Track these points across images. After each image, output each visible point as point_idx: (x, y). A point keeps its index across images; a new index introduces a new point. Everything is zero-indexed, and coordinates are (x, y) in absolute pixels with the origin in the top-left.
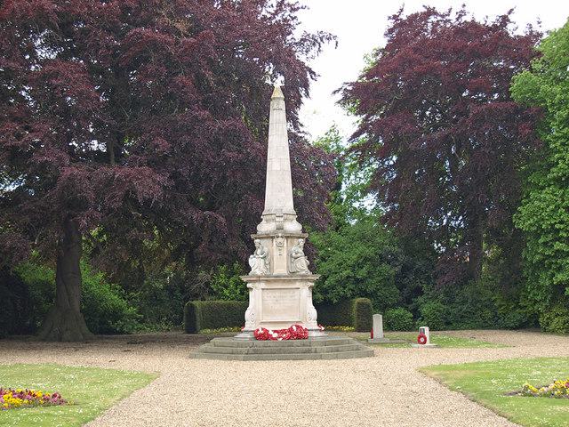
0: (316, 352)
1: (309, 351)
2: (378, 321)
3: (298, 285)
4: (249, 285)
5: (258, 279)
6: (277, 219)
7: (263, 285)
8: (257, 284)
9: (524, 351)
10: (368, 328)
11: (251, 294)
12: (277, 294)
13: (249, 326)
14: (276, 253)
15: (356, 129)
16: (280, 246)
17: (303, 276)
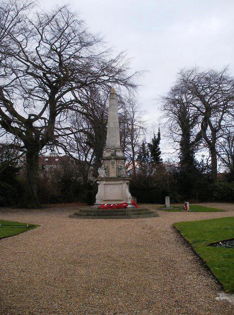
0: (128, 215)
1: (125, 215)
2: (167, 200)
3: (121, 182)
4: (98, 182)
5: (102, 179)
6: (112, 151)
7: (104, 182)
8: (101, 182)
9: (211, 215)
10: (163, 202)
11: (99, 186)
12: (113, 186)
13: (98, 202)
14: (111, 166)
15: (39, 126)
16: (113, 163)
17: (124, 178)
